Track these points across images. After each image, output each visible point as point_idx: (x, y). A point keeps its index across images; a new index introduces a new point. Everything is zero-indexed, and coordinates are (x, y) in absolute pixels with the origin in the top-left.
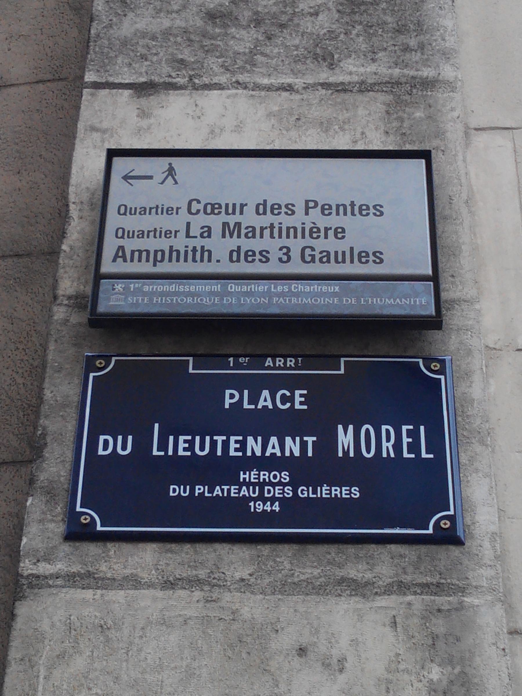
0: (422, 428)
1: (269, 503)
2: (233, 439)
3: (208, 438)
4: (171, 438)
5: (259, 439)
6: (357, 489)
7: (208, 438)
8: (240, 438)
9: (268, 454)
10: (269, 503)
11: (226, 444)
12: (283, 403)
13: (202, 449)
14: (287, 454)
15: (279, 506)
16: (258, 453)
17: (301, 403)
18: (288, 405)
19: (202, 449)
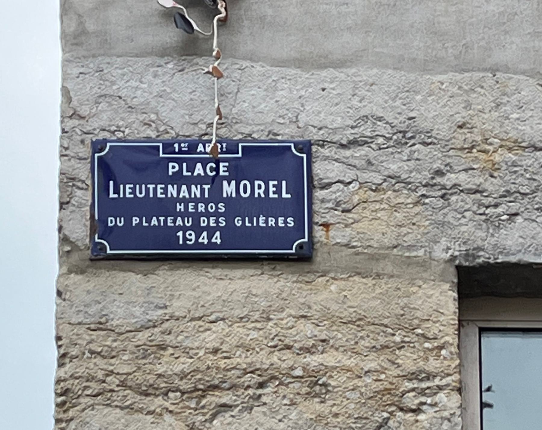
0: (284, 183)
1: (205, 234)
2: (159, 186)
3: (143, 186)
4: (122, 186)
5: (175, 186)
6: (292, 219)
7: (143, 186)
8: (276, 183)
9: (181, 196)
10: (205, 234)
11: (155, 190)
12: (211, 172)
13: (141, 193)
14: (193, 196)
15: (221, 238)
16: (175, 195)
17: (224, 171)
18: (214, 173)
19: (141, 193)
